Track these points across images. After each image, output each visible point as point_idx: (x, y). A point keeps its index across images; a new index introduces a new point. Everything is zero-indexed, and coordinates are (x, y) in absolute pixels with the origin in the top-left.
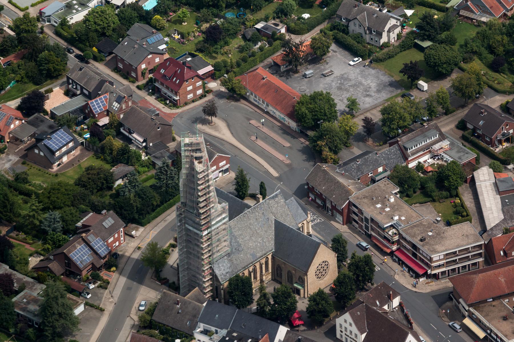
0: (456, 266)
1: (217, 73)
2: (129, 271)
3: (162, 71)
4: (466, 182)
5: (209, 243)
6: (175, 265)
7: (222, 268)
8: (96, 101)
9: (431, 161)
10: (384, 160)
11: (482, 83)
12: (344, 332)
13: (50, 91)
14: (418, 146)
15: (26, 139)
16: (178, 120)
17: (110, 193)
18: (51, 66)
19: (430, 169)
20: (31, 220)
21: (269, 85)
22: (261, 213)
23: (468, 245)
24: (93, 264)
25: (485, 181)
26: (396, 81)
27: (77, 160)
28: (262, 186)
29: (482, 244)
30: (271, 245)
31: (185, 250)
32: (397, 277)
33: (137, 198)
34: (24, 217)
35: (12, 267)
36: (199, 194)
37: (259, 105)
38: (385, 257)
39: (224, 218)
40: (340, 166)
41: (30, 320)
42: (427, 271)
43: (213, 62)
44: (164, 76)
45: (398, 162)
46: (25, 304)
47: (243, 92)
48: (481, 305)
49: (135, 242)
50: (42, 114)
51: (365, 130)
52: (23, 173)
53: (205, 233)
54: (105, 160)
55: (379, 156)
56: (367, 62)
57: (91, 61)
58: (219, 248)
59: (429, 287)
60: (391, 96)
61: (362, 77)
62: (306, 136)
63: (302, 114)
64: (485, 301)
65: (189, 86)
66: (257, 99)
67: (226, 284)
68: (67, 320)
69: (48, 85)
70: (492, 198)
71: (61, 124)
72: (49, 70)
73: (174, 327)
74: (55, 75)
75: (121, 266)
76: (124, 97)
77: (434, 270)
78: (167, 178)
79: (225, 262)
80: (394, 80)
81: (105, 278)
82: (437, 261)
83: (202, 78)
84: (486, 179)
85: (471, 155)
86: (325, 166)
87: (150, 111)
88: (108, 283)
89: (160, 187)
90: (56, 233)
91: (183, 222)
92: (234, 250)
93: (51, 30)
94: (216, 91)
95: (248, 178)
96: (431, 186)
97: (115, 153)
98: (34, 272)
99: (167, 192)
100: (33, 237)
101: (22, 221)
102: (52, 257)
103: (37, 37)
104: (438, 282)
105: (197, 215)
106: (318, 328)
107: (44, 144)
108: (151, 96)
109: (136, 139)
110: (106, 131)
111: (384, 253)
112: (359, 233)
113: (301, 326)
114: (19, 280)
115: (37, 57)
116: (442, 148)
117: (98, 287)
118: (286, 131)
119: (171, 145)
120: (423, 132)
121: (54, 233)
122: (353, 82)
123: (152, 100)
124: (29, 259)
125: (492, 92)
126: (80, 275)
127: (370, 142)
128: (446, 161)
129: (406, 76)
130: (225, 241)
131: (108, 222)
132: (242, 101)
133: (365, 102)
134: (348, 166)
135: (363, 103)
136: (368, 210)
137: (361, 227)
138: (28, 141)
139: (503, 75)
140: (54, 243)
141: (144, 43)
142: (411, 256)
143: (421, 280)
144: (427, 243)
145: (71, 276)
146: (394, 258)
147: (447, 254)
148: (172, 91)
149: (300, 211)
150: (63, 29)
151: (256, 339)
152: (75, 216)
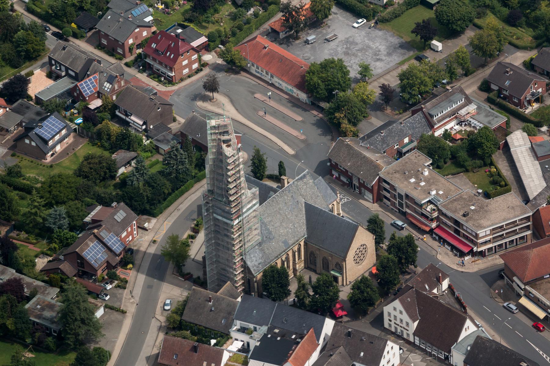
0: (503, 242)
1: (212, 44)
3: (154, 46)
4: (499, 149)
5: (240, 233)
6: (201, 259)
7: (254, 259)
8: (86, 83)
9: (457, 128)
10: (410, 129)
11: (502, 39)
12: (393, 321)
13: (31, 73)
14: (444, 112)
15: (12, 129)
16: (176, 98)
17: (114, 182)
18: (29, 46)
19: (459, 136)
20: (32, 217)
21: (272, 55)
22: (290, 196)
23: (515, 217)
24: (108, 262)
25: (520, 146)
26: (406, 42)
27: (72, 148)
28: (281, 166)
29: (529, 216)
30: (302, 230)
31: (213, 241)
32: (439, 257)
33: (147, 187)
34: (24, 215)
35: (19, 271)
36: (229, 180)
37: (262, 77)
38: (425, 236)
39: (254, 205)
40: (363, 139)
41: (47, 328)
42: (473, 248)
43: (206, 32)
44: (156, 50)
45: (424, 131)
46: (39, 311)
47: (243, 63)
48: (537, 283)
49: (151, 234)
50: (26, 100)
51: (384, 97)
52: (16, 166)
53: (236, 222)
54: (102, 146)
55: (404, 126)
56: (372, 23)
57: (71, 39)
58: (250, 238)
59: (476, 266)
60: (404, 58)
61: (369, 40)
62: (321, 110)
63: (315, 84)
64: (542, 278)
65: (184, 60)
66: (260, 71)
67: (259, 276)
68: (91, 326)
69: (27, 67)
70: (530, 165)
71: (50, 110)
72: (27, 51)
73: (207, 326)
74: (34, 56)
75: (137, 262)
76: (117, 76)
77: (480, 247)
78: (177, 163)
79: (256, 252)
80: (404, 41)
81: (122, 276)
82: (483, 237)
83: (197, 50)
84: (521, 144)
85: (500, 119)
86: (348, 141)
87: (146, 90)
88: (127, 282)
89: (170, 174)
90: (63, 231)
91: (211, 211)
92: (265, 239)
93: (22, 7)
94: (213, 64)
95: (265, 158)
96: (463, 154)
97: (114, 138)
98: (44, 274)
99: (176, 177)
100: (36, 236)
101: (19, 218)
102: (62, 257)
103: (11, 16)
104: (485, 260)
105: (227, 202)
106: (362, 318)
107: (36, 133)
108: (142, 73)
109: (134, 122)
110: (99, 114)
111: (423, 232)
112: (392, 211)
113: (344, 317)
114: (29, 285)
115: (12, 37)
116: (469, 113)
117: (116, 287)
118: (295, 103)
119: (173, 126)
120: (447, 97)
121: (61, 230)
122: (360, 46)
123: (143, 77)
124: (36, 261)
125: (512, 48)
126: (95, 275)
127: (389, 110)
128: (474, 127)
129: (419, 37)
130: (255, 229)
131: (120, 216)
132: (243, 73)
133: (377, 68)
134: (372, 138)
135: (375, 68)
136: (402, 185)
137: (393, 204)
138: (15, 131)
139: (521, 29)
140: (61, 242)
141: (130, 16)
142: (453, 233)
143: (467, 258)
144: (471, 218)
145: (84, 276)
146: (434, 236)
147: (493, 229)
148: (166, 67)
149: (330, 191)
150: (34, 4)
151: (300, 334)
152: (82, 210)
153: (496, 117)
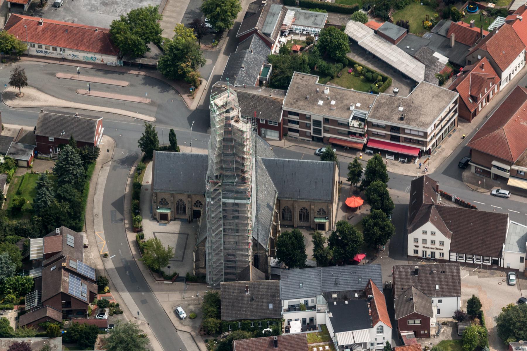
2: (122, 284)
25: (365, 36)
37: (47, 55)
63: (134, 42)
73: (254, 318)
118: (105, 70)
132: (23, 58)
140: (15, 290)
153: (316, 16)
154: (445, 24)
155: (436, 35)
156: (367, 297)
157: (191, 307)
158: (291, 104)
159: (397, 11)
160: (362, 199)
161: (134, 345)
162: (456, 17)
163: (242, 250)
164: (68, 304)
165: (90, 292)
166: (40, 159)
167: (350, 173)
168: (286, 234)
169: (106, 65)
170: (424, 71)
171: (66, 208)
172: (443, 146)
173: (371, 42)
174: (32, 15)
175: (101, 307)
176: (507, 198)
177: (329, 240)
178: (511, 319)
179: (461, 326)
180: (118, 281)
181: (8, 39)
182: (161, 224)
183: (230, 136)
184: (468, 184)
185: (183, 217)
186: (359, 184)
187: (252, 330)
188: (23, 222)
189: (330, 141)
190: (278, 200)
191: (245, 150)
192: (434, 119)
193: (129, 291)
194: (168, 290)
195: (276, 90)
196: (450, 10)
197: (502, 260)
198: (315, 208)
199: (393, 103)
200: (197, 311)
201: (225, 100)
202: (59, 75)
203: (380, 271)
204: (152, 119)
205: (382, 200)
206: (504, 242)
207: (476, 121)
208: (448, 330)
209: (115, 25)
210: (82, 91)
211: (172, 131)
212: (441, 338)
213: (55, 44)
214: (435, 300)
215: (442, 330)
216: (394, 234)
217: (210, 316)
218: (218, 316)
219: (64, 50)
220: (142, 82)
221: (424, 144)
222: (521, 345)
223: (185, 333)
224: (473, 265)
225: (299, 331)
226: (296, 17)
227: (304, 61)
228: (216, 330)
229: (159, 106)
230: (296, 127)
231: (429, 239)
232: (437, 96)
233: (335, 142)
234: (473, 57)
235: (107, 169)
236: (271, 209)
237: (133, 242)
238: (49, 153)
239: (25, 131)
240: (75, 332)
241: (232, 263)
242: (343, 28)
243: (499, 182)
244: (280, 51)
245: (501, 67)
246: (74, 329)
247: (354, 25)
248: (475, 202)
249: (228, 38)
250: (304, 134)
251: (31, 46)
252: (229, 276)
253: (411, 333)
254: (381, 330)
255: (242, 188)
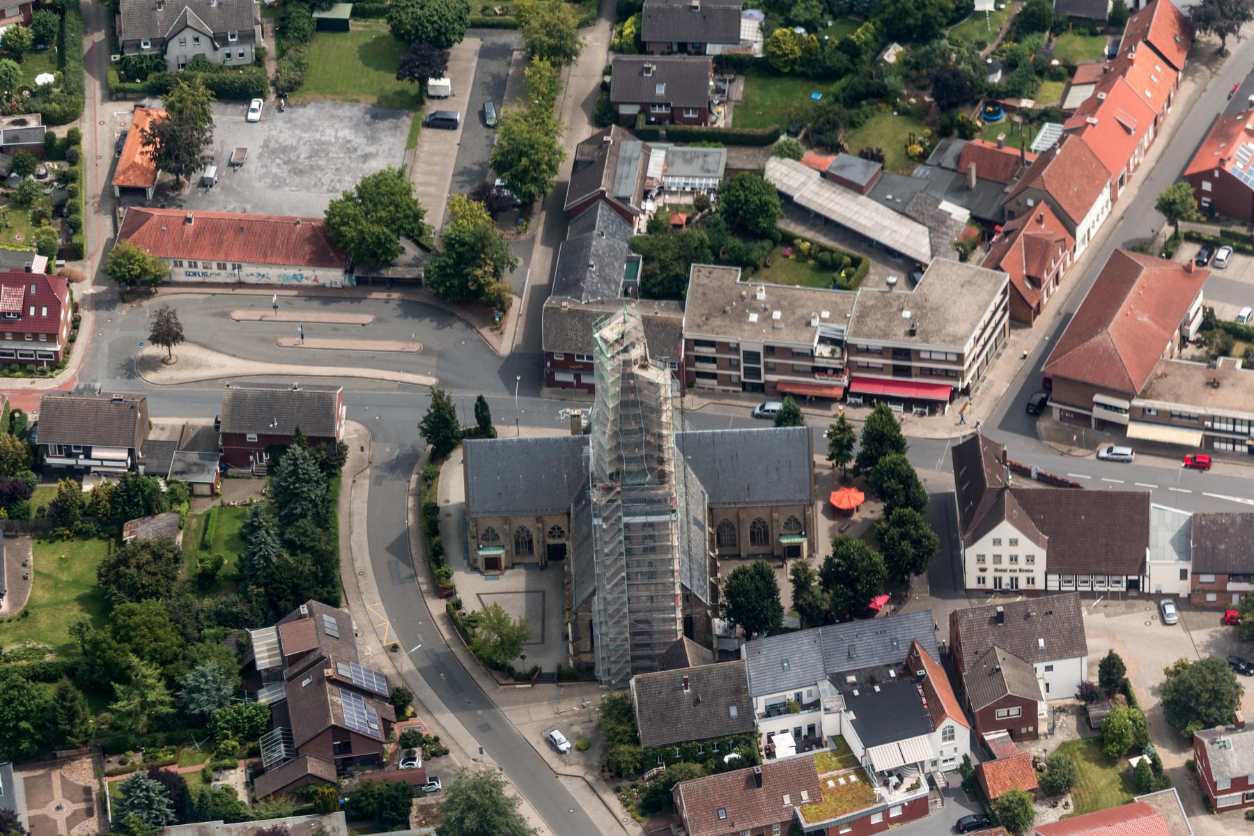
2: (437, 698)
25: (804, 184)
27: (18, 565)
37: (207, 280)
109: (102, 460)
118: (323, 296)
132: (161, 290)
140: (236, 729)
142: (889, 378)
148: (36, 337)
154: (951, 148)
155: (938, 170)
156: (913, 674)
157: (577, 729)
158: (699, 326)
159: (851, 132)
160: (860, 490)
161: (496, 812)
162: (967, 132)
163: (663, 610)
164: (345, 747)
165: (384, 720)
166: (233, 477)
167: (831, 445)
168: (743, 571)
169: (323, 286)
170: (928, 240)
171: (307, 564)
172: (990, 377)
173: (817, 194)
174: (163, 207)
175: (405, 746)
176: (1129, 461)
177: (820, 575)
178: (1191, 688)
179: (1094, 711)
180: (424, 691)
181: (133, 256)
182: (488, 577)
183: (632, 397)
184: (1052, 444)
185: (528, 560)
186: (850, 465)
187: (702, 760)
188: (227, 599)
189: (779, 388)
190: (711, 510)
191: (664, 418)
192: (973, 326)
193: (453, 711)
194: (526, 702)
195: (663, 303)
196: (952, 119)
197: (1146, 580)
198: (781, 517)
199: (888, 305)
200: (589, 735)
201: (620, 329)
202: (238, 314)
203: (923, 622)
204: (432, 381)
205: (907, 488)
206: (1147, 544)
207: (1043, 324)
208: (1069, 723)
209: (333, 211)
210: (286, 341)
211: (480, 399)
212: (1060, 737)
213: (222, 256)
214: (1040, 667)
215: (1059, 724)
216: (938, 551)
217: (621, 742)
218: (636, 741)
219: (240, 267)
220: (399, 312)
221: (958, 375)
222: (1220, 734)
223: (574, 778)
224: (1092, 595)
225: (792, 752)
226: (668, 162)
227: (702, 242)
228: (635, 767)
229: (440, 355)
230: (710, 368)
231: (1007, 553)
232: (969, 282)
233: (788, 390)
234: (1018, 204)
235: (365, 483)
236: (702, 528)
237: (442, 617)
238: (249, 464)
239: (193, 427)
240: (367, 798)
241: (646, 637)
242: (761, 172)
243: (1108, 434)
244: (648, 228)
245: (1073, 217)
246: (366, 791)
247: (779, 166)
248: (1072, 477)
249: (544, 213)
250: (727, 380)
251: (176, 265)
252: (639, 663)
253: (1004, 733)
254: (949, 735)
255: (661, 492)
